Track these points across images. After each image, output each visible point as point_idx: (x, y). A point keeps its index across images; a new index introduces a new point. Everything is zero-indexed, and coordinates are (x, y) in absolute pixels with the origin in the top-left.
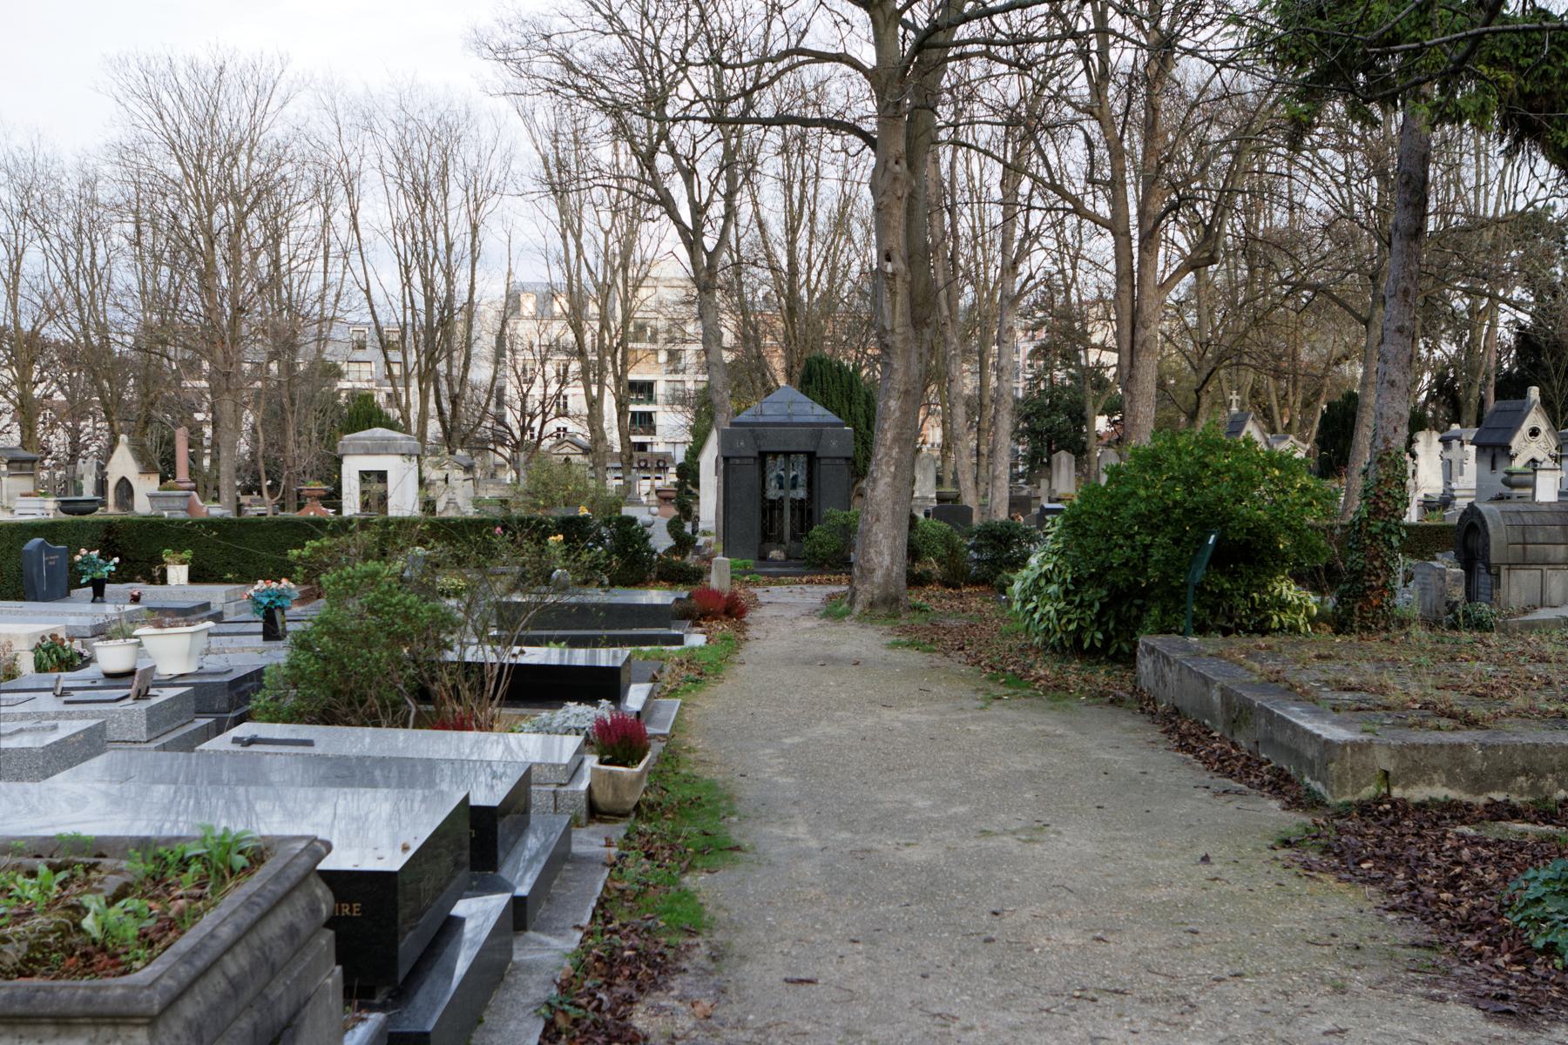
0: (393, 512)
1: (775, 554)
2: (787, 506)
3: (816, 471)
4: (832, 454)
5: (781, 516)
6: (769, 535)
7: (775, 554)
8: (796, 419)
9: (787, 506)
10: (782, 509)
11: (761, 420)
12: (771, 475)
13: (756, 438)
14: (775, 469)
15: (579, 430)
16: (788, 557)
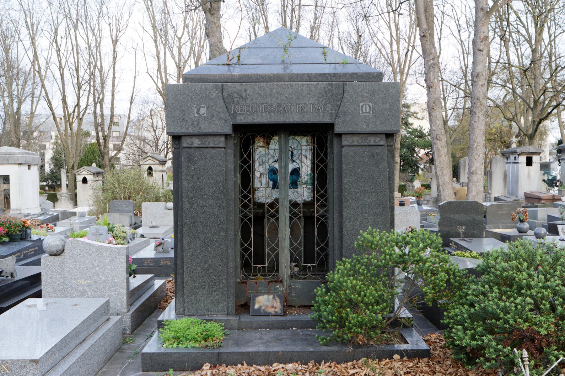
0: (144, 204)
1: (265, 302)
2: (284, 216)
3: (333, 158)
4: (364, 128)
5: (275, 230)
6: (255, 260)
7: (265, 302)
8: (296, 70)
9: (284, 216)
10: (275, 216)
11: (237, 71)
12: (260, 171)
13: (228, 101)
14: (265, 156)
15: (94, 141)
16: (287, 306)
